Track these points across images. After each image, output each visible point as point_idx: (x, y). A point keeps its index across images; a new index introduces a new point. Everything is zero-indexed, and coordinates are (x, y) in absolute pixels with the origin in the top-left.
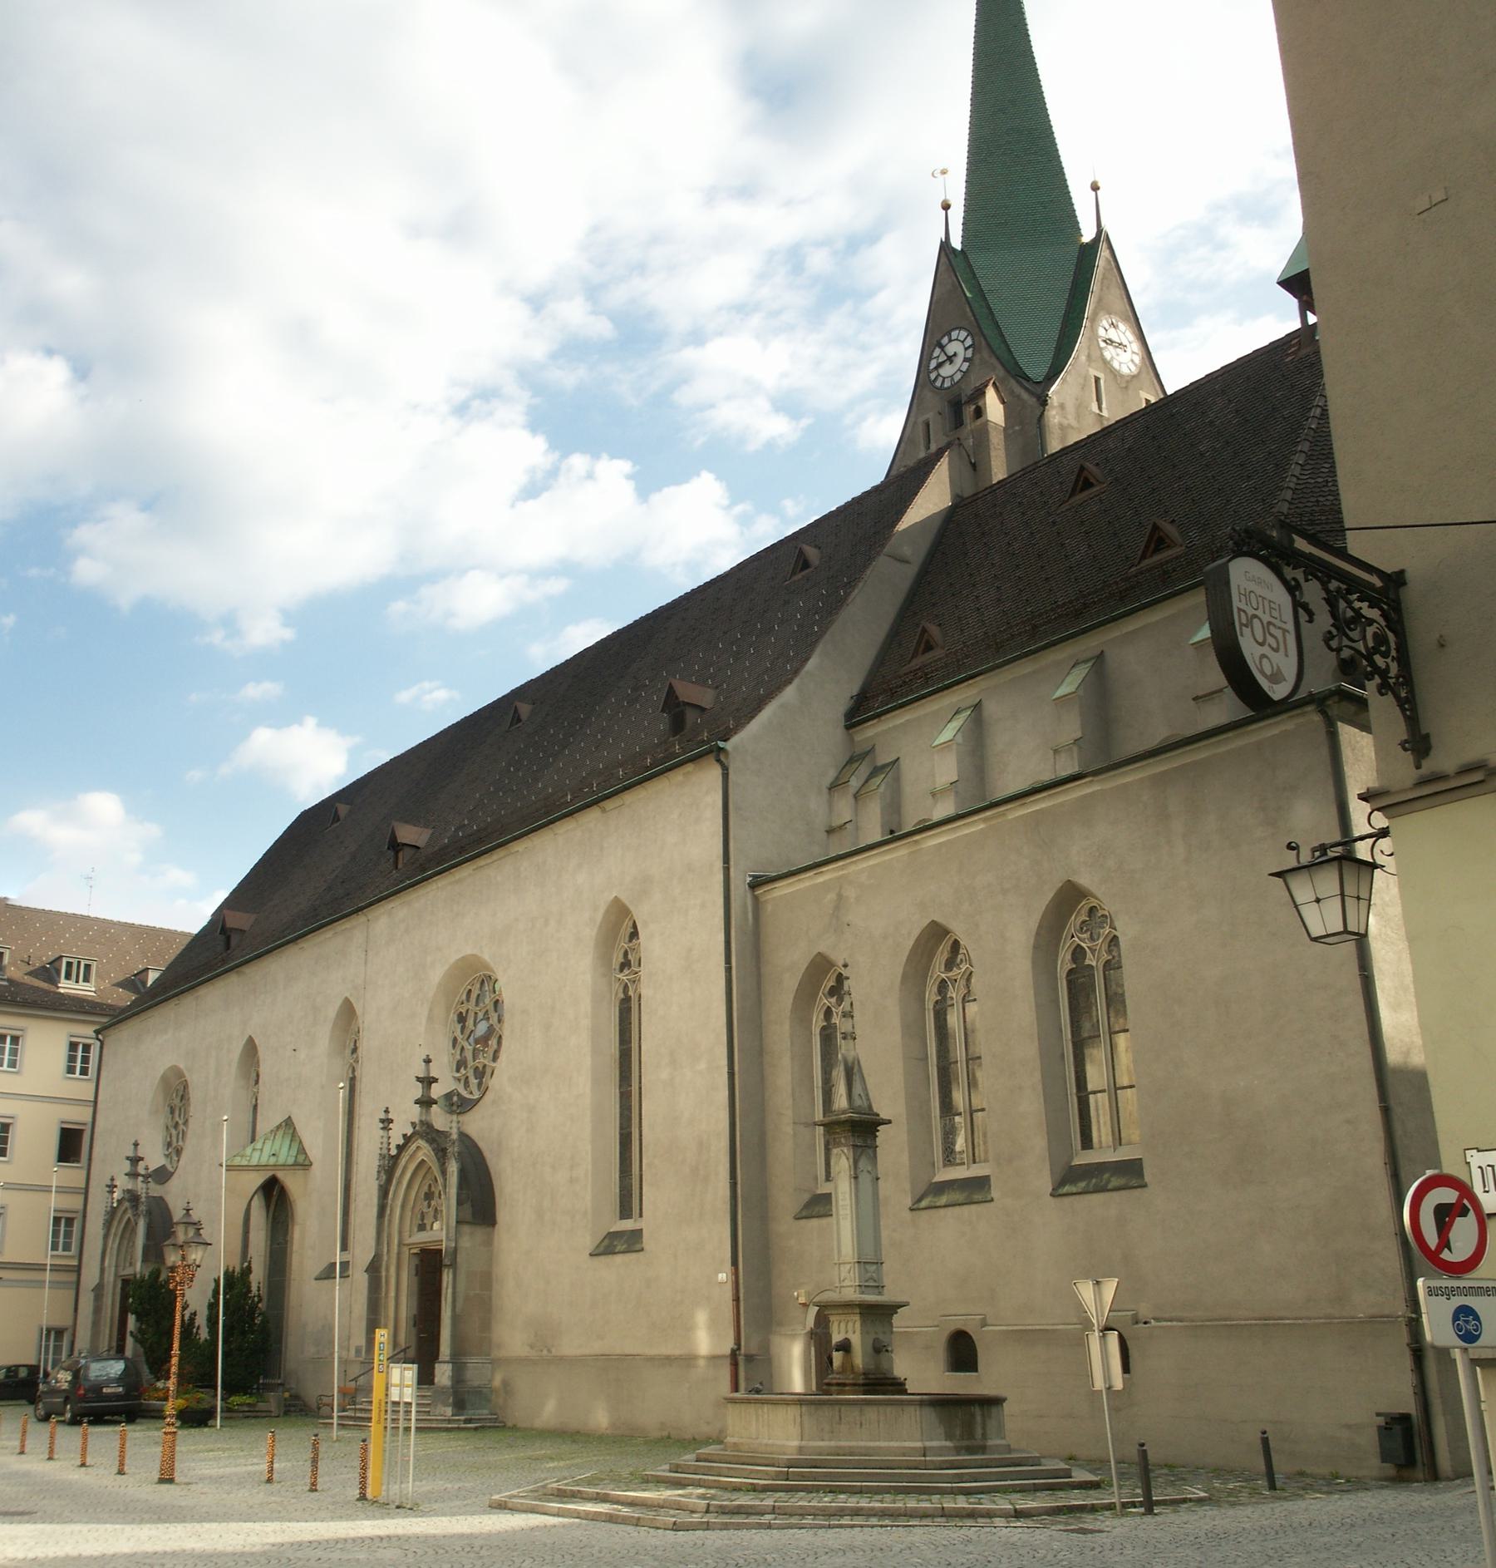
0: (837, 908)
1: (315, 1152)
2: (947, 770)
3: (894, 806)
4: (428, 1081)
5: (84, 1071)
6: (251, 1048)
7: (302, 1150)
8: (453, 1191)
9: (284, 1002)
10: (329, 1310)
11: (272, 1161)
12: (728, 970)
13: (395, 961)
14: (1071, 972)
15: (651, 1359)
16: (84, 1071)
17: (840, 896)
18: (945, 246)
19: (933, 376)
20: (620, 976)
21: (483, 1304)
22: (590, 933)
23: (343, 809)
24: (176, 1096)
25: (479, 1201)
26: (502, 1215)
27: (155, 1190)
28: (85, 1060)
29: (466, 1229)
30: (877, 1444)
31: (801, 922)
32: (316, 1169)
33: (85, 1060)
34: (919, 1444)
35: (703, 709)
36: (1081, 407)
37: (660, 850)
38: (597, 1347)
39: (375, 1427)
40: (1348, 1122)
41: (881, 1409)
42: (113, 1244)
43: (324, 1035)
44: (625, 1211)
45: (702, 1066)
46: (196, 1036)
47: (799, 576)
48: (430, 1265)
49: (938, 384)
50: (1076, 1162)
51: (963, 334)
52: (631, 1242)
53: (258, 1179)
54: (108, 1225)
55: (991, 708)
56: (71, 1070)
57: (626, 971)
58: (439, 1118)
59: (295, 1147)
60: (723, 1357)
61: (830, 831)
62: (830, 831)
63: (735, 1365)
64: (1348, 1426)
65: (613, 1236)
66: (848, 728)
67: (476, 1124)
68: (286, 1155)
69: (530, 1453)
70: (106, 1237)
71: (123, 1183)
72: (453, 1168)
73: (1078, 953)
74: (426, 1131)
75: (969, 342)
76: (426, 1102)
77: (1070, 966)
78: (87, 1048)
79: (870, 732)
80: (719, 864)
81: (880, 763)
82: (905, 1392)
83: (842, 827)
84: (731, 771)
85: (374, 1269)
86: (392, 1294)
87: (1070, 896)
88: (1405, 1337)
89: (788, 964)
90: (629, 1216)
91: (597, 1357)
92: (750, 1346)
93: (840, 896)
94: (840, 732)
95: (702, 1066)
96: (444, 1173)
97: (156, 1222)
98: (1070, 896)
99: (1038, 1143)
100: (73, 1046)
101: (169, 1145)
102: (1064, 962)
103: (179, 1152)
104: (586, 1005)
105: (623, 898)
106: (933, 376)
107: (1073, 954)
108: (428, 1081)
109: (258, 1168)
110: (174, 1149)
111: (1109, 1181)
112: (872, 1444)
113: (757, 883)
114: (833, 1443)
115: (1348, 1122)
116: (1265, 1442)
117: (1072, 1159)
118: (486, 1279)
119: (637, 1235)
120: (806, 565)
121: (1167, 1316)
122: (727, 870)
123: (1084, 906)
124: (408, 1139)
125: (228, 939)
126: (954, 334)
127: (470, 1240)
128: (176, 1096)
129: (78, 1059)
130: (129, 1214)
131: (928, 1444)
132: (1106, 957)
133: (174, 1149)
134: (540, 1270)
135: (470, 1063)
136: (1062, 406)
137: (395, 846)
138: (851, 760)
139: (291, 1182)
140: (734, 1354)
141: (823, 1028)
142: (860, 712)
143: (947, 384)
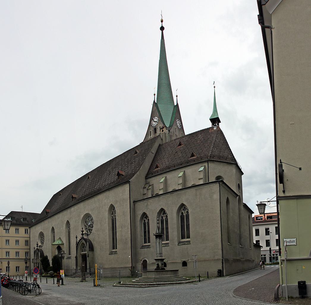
0: (147, 206)
1: (64, 242)
2: (162, 186)
3: (153, 191)
4: (83, 231)
5: (27, 233)
6: (53, 228)
7: (62, 242)
8: (88, 246)
9: (58, 222)
10: (70, 262)
11: (59, 243)
12: (130, 214)
13: (75, 214)
14: (181, 216)
16: (27, 233)
17: (147, 204)
18: (154, 101)
19: (152, 124)
21: (93, 262)
22: (107, 209)
23: (61, 194)
24: (42, 235)
25: (92, 248)
26: (95, 250)
27: (41, 248)
28: (27, 232)
29: (90, 252)
31: (141, 208)
32: (65, 244)
33: (27, 232)
35: (123, 175)
36: (173, 132)
37: (121, 196)
39: (280, 265)
42: (35, 256)
43: (64, 226)
45: (126, 228)
46: (44, 227)
47: (136, 155)
48: (84, 257)
49: (153, 126)
51: (157, 118)
52: (116, 253)
53: (57, 246)
54: (34, 253)
55: (168, 177)
56: (26, 233)
58: (85, 237)
59: (61, 241)
61: (143, 194)
62: (143, 194)
66: (145, 179)
67: (91, 237)
68: (60, 243)
69: (246, 277)
70: (34, 255)
71: (36, 248)
72: (88, 243)
73: (182, 213)
74: (83, 238)
75: (158, 119)
76: (83, 234)
77: (181, 215)
78: (27, 230)
79: (149, 180)
80: (129, 199)
81: (150, 185)
82: (165, 270)
83: (145, 194)
84: (131, 185)
85: (76, 257)
86: (79, 260)
87: (183, 205)
88: (221, 261)
89: (139, 213)
91: (110, 268)
92: (134, 265)
93: (147, 204)
94: (144, 179)
95: (126, 228)
96: (87, 244)
97: (39, 252)
98: (183, 205)
99: (176, 238)
100: (25, 230)
101: (41, 242)
102: (180, 214)
103: (43, 243)
104: (107, 220)
105: (113, 204)
106: (152, 124)
108: (83, 231)
109: (57, 244)
110: (42, 243)
113: (134, 202)
118: (93, 258)
120: (137, 153)
122: (130, 200)
123: (184, 207)
124: (80, 240)
125: (47, 213)
126: (155, 117)
127: (90, 253)
128: (42, 235)
129: (26, 232)
130: (38, 251)
133: (42, 243)
134: (102, 256)
135: (88, 229)
136: (171, 132)
137: (73, 197)
138: (146, 184)
139: (61, 246)
140: (131, 266)
141: (144, 223)
142: (147, 177)
143: (154, 126)
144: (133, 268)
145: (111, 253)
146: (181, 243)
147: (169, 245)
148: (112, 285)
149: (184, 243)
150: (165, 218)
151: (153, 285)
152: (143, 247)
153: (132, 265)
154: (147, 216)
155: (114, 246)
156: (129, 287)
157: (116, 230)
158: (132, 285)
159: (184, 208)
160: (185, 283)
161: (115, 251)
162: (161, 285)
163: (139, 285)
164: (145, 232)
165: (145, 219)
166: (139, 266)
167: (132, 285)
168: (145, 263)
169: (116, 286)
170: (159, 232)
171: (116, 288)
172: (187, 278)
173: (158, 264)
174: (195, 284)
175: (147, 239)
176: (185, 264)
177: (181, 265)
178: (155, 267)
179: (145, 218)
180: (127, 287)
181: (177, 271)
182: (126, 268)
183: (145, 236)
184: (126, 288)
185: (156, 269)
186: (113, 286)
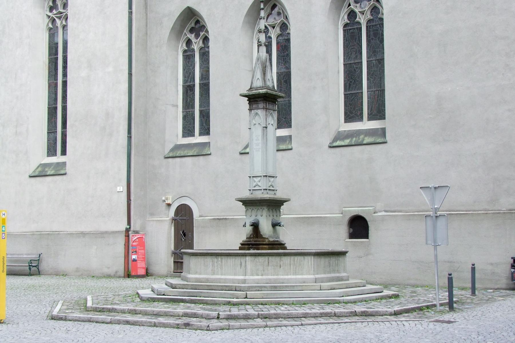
12: (130, 13)
15: (71, 234)
20: (50, 14)
30: (289, 277)
34: (312, 276)
38: (33, 227)
40: (509, 110)
41: (292, 258)
44: (51, 151)
45: (110, 69)
50: (341, 129)
52: (59, 171)
57: (55, 12)
60: (122, 232)
63: (127, 236)
64: (492, 264)
65: (340, 136)
82: (285, 248)
90: (359, 118)
91: (33, 234)
95: (110, 69)
107: (349, 15)
111: (363, 140)
112: (286, 277)
114: (275, 277)
115: (509, 110)
116: (473, 269)
117: (339, 128)
119: (383, 132)
121: (393, 209)
131: (317, 276)
132: (369, 17)
140: (127, 230)
144: (132, 240)
145: (41, 173)
146: (343, 139)
147: (294, 145)
148: (45, 311)
149: (354, 140)
150: (369, 17)
151: (247, 317)
152: (177, 153)
153: (129, 223)
154: (198, 22)
155: (57, 141)
156: (128, 322)
157: (65, 75)
158: (145, 313)
159: (193, 25)
160: (391, 315)
161: (58, 164)
162: (285, 322)
163: (179, 316)
164: (188, 90)
165: (192, 37)
166: (160, 238)
167: (145, 313)
168: (184, 223)
169: (65, 319)
170: (264, 80)
171: (68, 331)
172: (386, 292)
173: (255, 226)
174: (437, 321)
175: (197, 114)
176: (359, 227)
177: (344, 230)
178: (244, 234)
179: (192, 31)
180: (119, 322)
181: (341, 259)
182: (103, 234)
183: (188, 103)
184: (117, 327)
185: (245, 246)
186: (53, 318)
